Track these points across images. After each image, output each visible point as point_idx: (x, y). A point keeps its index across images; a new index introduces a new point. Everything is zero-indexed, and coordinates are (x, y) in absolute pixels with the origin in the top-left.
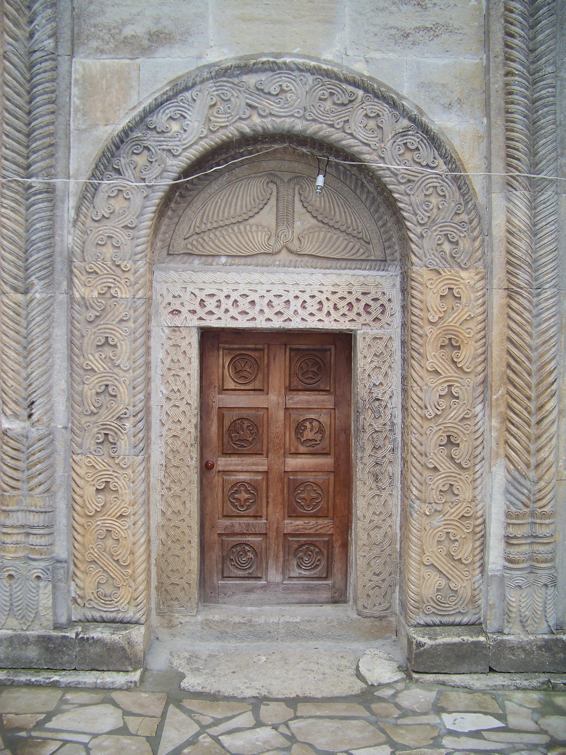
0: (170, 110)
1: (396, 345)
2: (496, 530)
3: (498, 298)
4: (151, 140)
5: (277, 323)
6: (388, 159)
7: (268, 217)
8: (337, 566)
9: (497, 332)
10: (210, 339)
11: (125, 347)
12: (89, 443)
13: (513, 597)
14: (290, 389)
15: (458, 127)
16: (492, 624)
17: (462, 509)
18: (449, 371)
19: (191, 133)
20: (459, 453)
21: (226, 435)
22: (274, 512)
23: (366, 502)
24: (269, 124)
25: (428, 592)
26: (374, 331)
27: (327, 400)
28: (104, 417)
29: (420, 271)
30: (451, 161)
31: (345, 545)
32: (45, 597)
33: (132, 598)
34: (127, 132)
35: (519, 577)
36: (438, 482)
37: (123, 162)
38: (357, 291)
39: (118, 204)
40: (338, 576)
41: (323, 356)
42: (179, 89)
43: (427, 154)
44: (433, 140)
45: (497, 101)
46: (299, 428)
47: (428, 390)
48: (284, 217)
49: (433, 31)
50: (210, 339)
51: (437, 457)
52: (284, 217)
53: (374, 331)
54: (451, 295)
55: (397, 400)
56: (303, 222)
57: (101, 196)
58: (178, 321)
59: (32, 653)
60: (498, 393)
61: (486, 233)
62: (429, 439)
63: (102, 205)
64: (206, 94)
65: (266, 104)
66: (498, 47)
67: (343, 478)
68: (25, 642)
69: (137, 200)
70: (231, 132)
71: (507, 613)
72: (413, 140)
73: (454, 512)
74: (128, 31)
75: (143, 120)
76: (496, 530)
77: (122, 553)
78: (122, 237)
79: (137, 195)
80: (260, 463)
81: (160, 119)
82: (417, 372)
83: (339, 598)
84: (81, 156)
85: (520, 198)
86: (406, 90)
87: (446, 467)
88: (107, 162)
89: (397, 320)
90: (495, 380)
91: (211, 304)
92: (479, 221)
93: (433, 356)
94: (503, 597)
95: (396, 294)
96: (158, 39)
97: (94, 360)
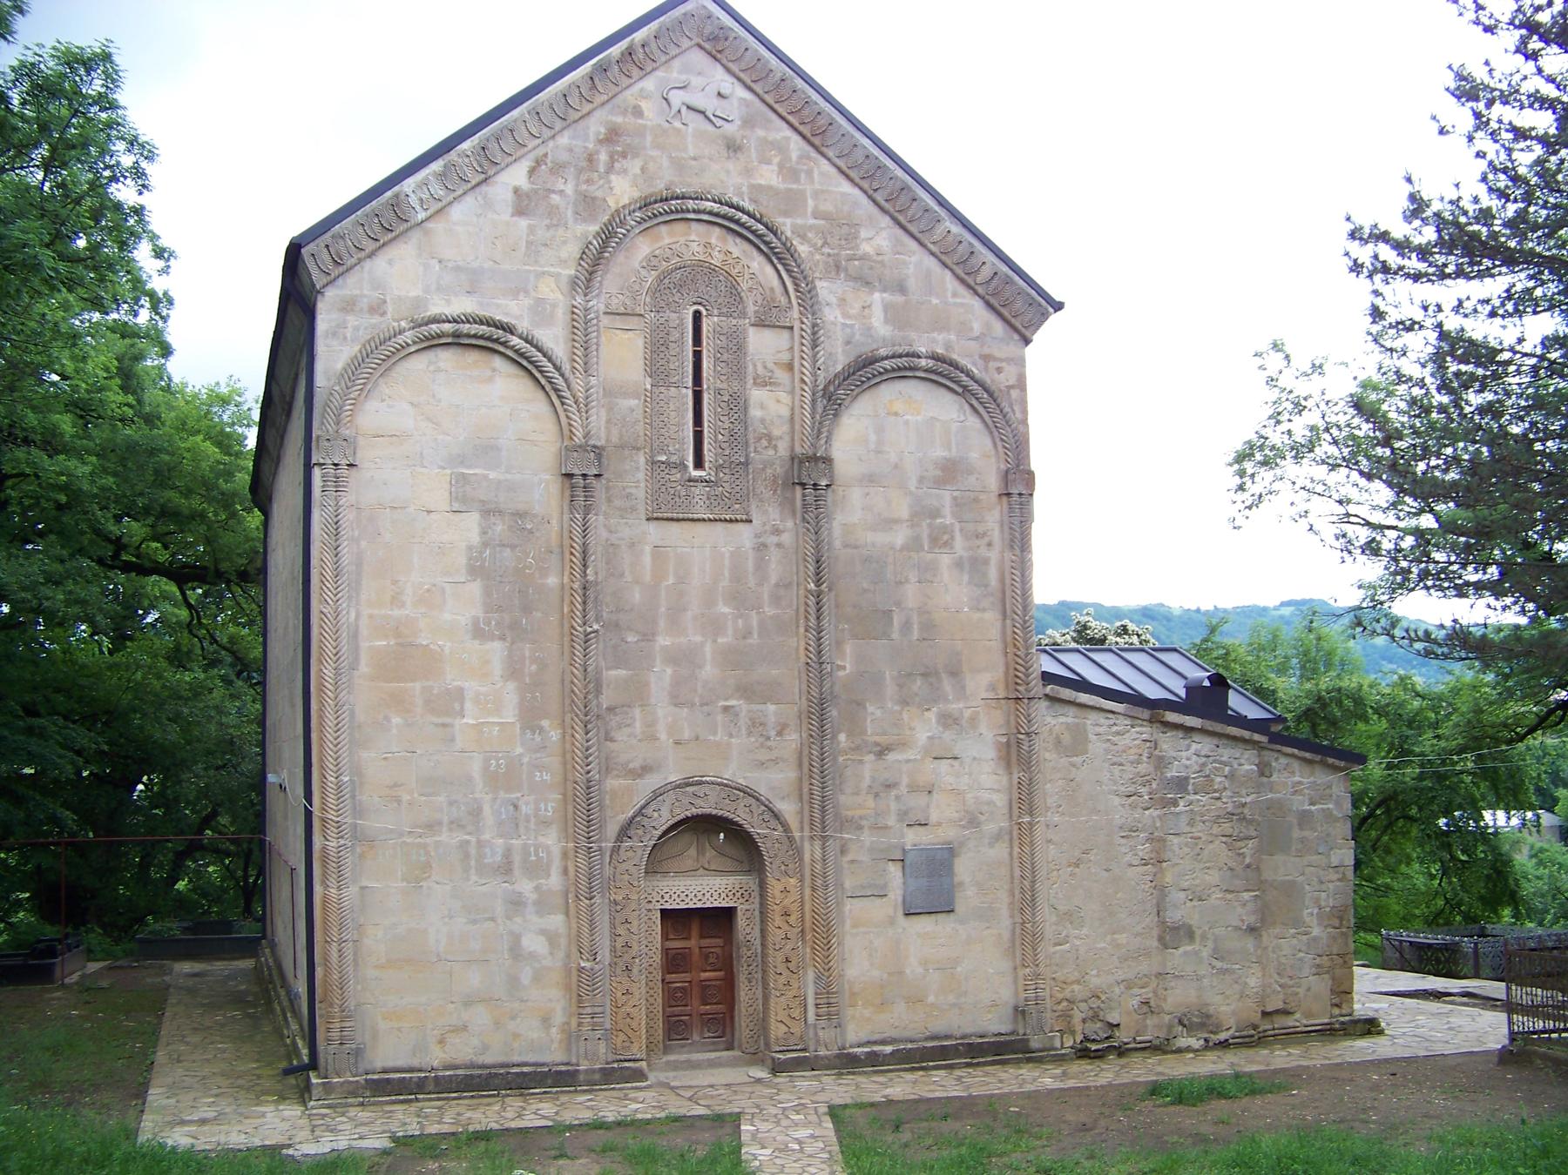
0: (653, 806)
1: (757, 913)
2: (811, 1001)
3: (808, 891)
4: (645, 821)
5: (699, 905)
6: (757, 830)
7: (693, 852)
8: (728, 1030)
9: (807, 907)
10: (665, 913)
11: (635, 923)
12: (619, 971)
13: (821, 1033)
14: (702, 937)
15: (788, 808)
16: (812, 1048)
17: (794, 992)
18: (786, 927)
19: (664, 817)
20: (792, 966)
21: (673, 962)
22: (696, 1002)
23: (746, 994)
24: (700, 811)
25: (780, 1034)
26: (746, 907)
27: (719, 942)
28: (627, 957)
29: (770, 880)
30: (786, 828)
31: (732, 1018)
32: (602, 1048)
33: (638, 1050)
34: (633, 818)
35: (823, 1023)
36: (782, 980)
37: (631, 833)
38: (737, 887)
39: (630, 854)
40: (728, 1035)
41: (719, 919)
42: (657, 795)
43: (773, 823)
44: (776, 816)
45: (806, 797)
46: (707, 957)
47: (775, 936)
48: (701, 852)
49: (775, 761)
50: (665, 913)
51: (781, 968)
52: (701, 852)
53: (746, 907)
54: (785, 890)
55: (758, 942)
56: (710, 853)
57: (622, 851)
58: (650, 906)
59: (597, 1077)
60: (447, 720)
61: (801, 859)
62: (776, 959)
63: (623, 855)
64: (670, 798)
65: (698, 802)
66: (806, 770)
67: (730, 983)
68: (594, 1071)
69: (640, 852)
70: (682, 816)
71: (818, 1041)
72: (767, 818)
73: (791, 994)
74: (631, 766)
75: (640, 812)
76: (811, 1001)
77: (634, 1025)
78: (633, 870)
79: (639, 849)
80: (686, 976)
81: (648, 811)
82: (771, 928)
83: (730, 1047)
84: (612, 829)
85: (817, 844)
86: (762, 790)
87: (786, 973)
88: (624, 832)
89: (757, 900)
90: (807, 930)
91: (667, 897)
92: (799, 852)
93: (778, 921)
94: (816, 1034)
95: (755, 887)
96: (646, 770)
97: (620, 930)
